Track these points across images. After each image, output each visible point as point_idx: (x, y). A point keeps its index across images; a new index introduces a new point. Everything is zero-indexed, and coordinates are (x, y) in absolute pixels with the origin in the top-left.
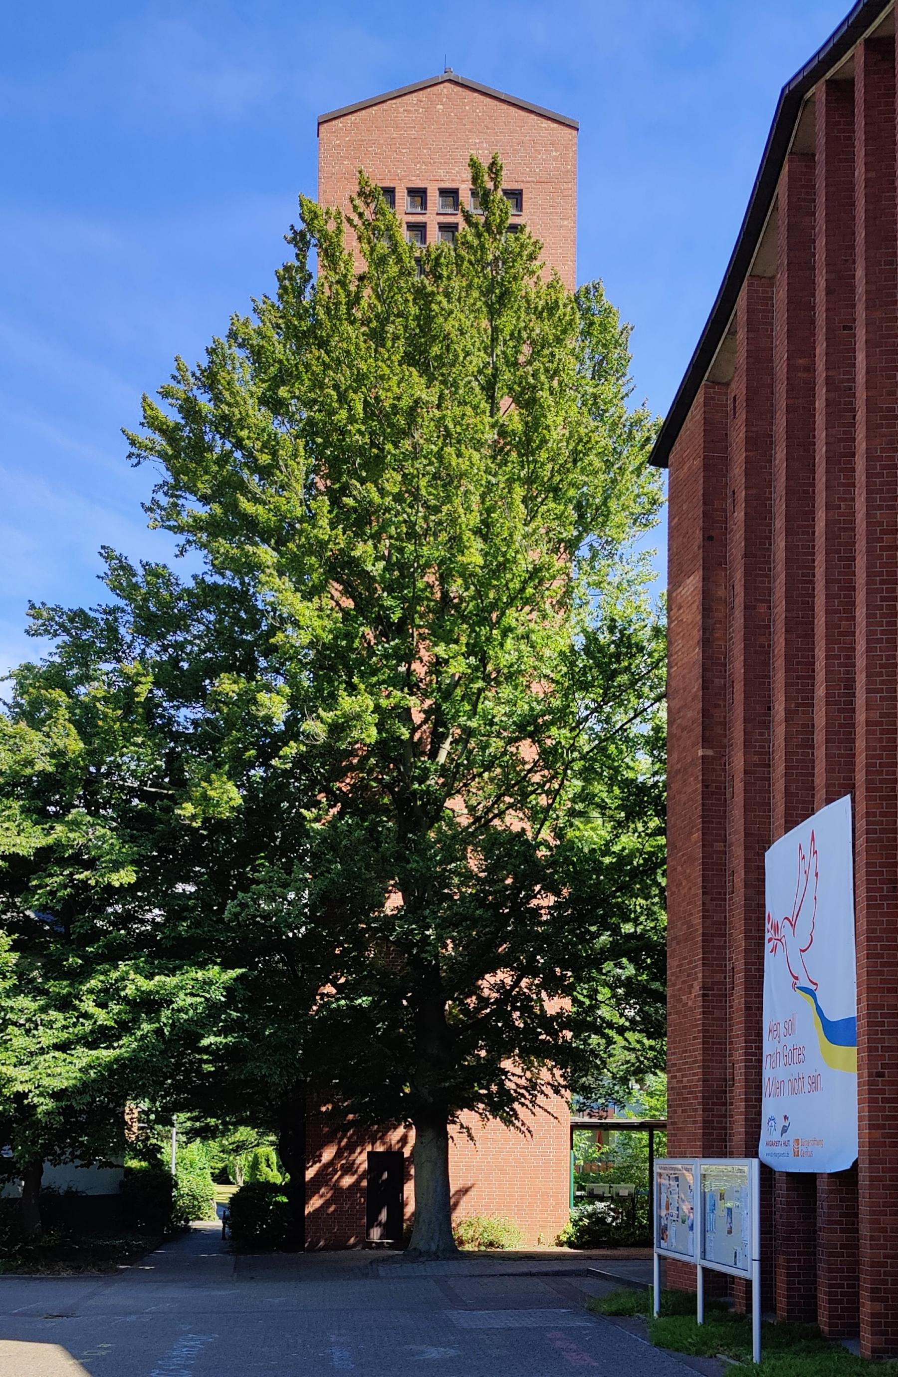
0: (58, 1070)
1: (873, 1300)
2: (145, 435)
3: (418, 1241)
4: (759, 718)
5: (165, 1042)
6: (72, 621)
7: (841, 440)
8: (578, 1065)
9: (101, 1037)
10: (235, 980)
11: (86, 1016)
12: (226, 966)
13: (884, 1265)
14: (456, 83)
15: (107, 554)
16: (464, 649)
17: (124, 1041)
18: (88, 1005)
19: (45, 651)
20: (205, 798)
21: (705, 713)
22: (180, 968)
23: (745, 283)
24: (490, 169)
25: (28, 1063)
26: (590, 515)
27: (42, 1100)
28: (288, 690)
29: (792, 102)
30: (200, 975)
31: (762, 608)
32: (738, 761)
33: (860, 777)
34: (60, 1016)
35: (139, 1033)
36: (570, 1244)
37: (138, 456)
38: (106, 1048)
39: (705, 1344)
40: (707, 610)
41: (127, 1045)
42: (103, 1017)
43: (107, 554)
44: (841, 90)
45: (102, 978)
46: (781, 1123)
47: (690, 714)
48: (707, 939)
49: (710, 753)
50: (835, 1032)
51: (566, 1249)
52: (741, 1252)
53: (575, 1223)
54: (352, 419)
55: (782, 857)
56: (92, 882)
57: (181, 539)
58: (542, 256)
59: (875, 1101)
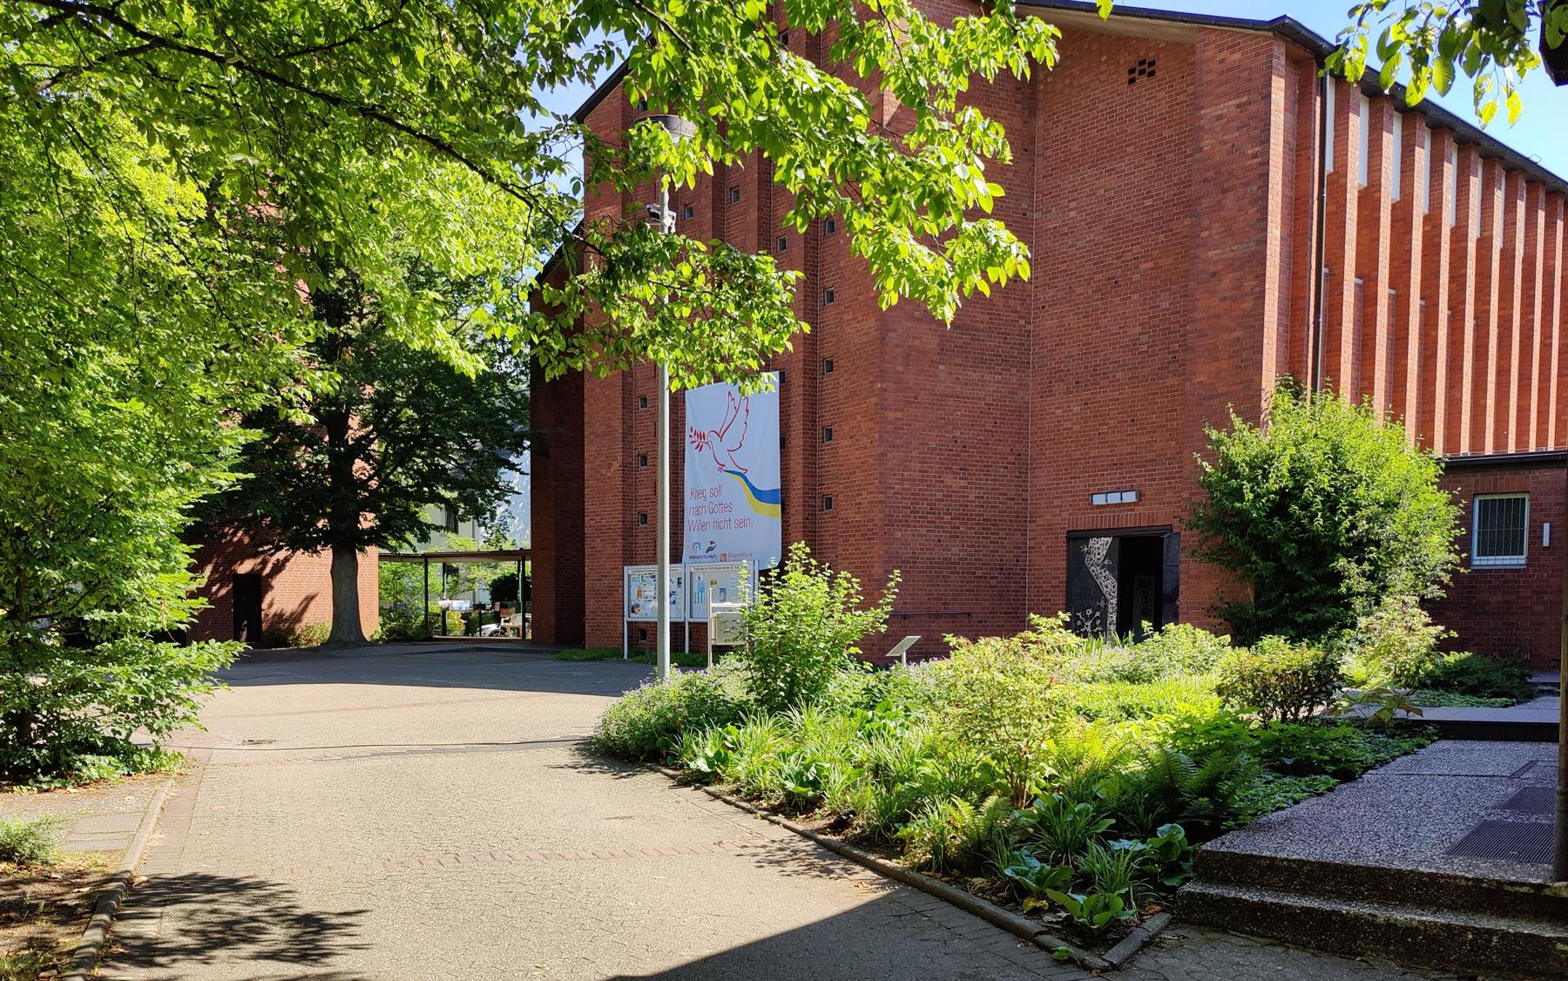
50: (759, 495)
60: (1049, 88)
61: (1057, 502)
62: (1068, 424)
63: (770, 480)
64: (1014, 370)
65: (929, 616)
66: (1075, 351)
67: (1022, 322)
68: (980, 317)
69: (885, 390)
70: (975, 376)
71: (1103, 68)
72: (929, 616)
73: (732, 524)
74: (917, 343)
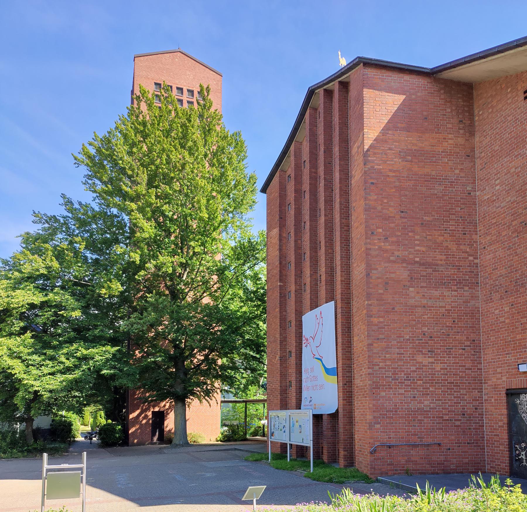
0: (52, 382)
1: (344, 451)
2: (80, 157)
3: (175, 441)
4: (299, 274)
5: (91, 373)
6: (50, 219)
7: (328, 196)
8: (230, 381)
9: (68, 370)
10: (117, 351)
11: (62, 363)
12: (113, 346)
13: (347, 440)
14: (182, 53)
15: (63, 196)
16: (200, 244)
17: (76, 372)
18: (63, 359)
19: (35, 229)
20: (109, 287)
21: (280, 271)
22: (96, 346)
23: (293, 143)
24: (207, 89)
25: (38, 380)
26: (238, 205)
27: (45, 393)
28: (140, 253)
29: (311, 93)
30: (104, 349)
31: (299, 242)
32: (293, 288)
33: (339, 297)
34: (51, 363)
35: (82, 369)
36: (221, 441)
37: (78, 164)
38: (69, 374)
39: (293, 467)
40: (280, 240)
41: (77, 374)
42: (68, 363)
43: (63, 196)
44: (329, 93)
45: (67, 349)
46: (309, 399)
47: (275, 271)
48: (281, 342)
49: (282, 284)
50: (328, 371)
51: (219, 442)
52: (306, 438)
53: (222, 434)
54: (161, 163)
55: (309, 319)
56: (65, 315)
57: (95, 195)
58: (222, 120)
59: (344, 392)
60: (481, 117)
61: (499, 370)
62: (502, 319)
63: (332, 363)
64: (466, 288)
65: (409, 446)
66: (503, 271)
67: (471, 258)
68: (439, 257)
69: (371, 305)
70: (436, 293)
71: (509, 96)
72: (409, 446)
73: (318, 388)
74: (393, 275)
